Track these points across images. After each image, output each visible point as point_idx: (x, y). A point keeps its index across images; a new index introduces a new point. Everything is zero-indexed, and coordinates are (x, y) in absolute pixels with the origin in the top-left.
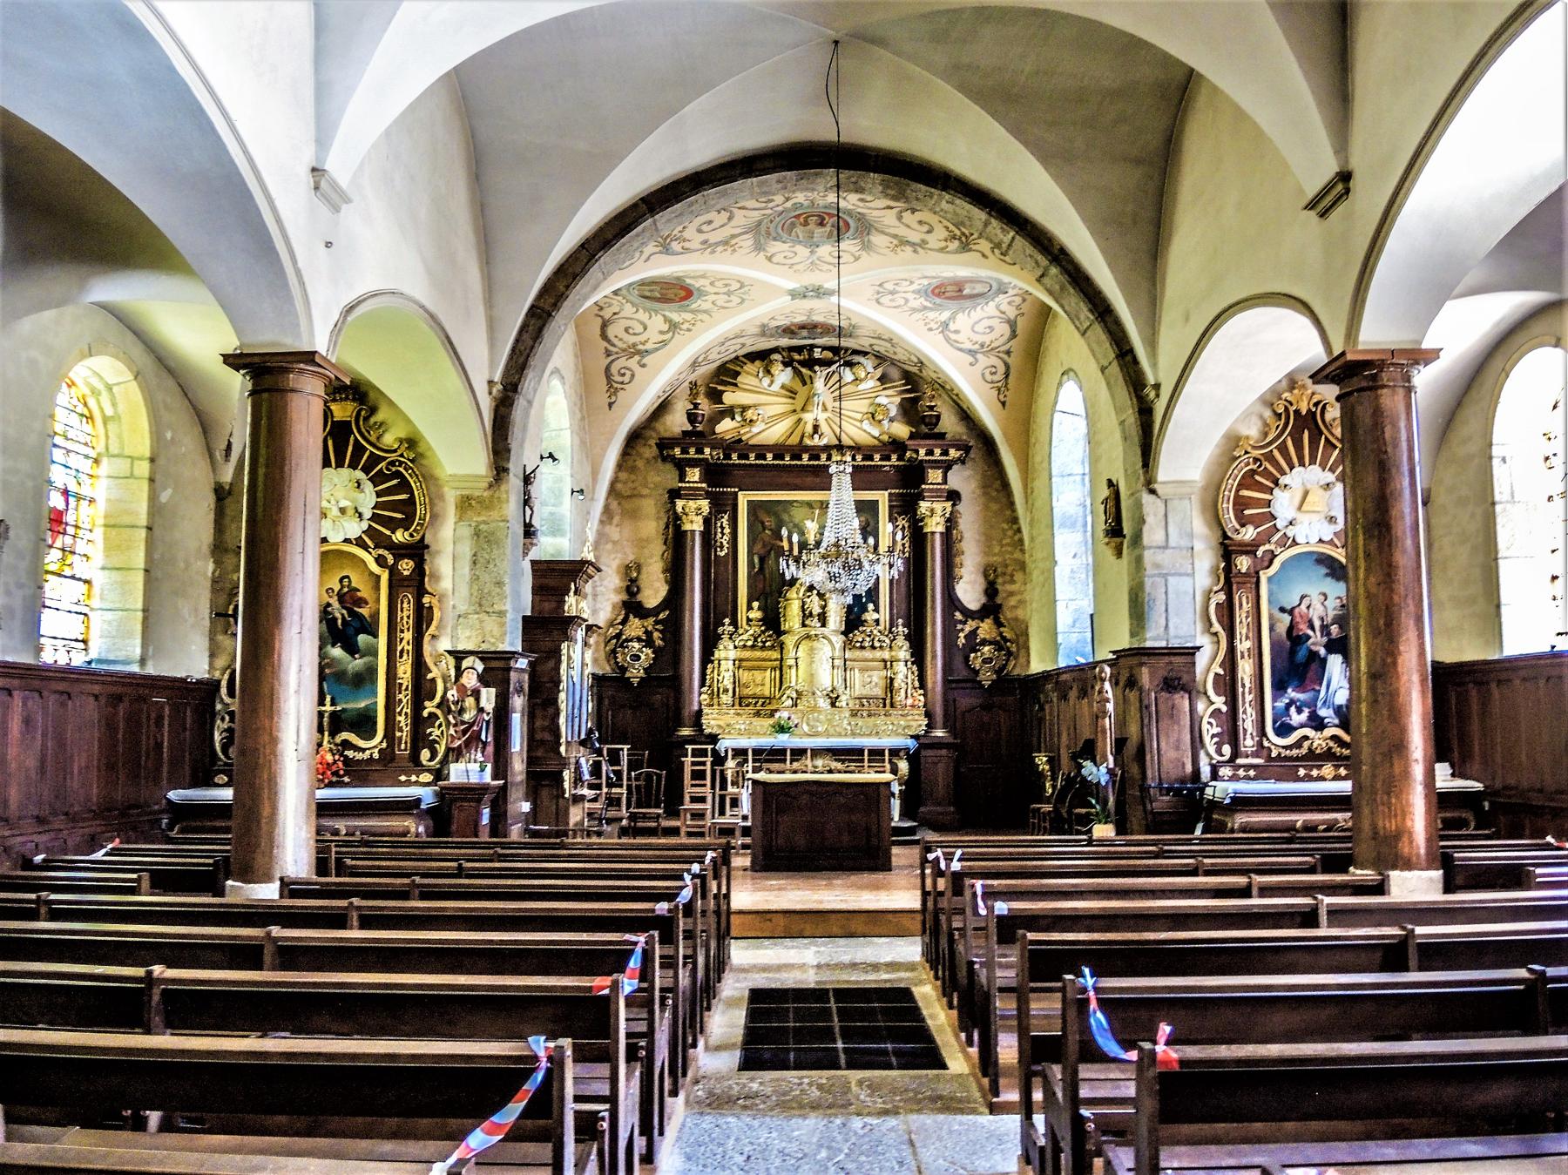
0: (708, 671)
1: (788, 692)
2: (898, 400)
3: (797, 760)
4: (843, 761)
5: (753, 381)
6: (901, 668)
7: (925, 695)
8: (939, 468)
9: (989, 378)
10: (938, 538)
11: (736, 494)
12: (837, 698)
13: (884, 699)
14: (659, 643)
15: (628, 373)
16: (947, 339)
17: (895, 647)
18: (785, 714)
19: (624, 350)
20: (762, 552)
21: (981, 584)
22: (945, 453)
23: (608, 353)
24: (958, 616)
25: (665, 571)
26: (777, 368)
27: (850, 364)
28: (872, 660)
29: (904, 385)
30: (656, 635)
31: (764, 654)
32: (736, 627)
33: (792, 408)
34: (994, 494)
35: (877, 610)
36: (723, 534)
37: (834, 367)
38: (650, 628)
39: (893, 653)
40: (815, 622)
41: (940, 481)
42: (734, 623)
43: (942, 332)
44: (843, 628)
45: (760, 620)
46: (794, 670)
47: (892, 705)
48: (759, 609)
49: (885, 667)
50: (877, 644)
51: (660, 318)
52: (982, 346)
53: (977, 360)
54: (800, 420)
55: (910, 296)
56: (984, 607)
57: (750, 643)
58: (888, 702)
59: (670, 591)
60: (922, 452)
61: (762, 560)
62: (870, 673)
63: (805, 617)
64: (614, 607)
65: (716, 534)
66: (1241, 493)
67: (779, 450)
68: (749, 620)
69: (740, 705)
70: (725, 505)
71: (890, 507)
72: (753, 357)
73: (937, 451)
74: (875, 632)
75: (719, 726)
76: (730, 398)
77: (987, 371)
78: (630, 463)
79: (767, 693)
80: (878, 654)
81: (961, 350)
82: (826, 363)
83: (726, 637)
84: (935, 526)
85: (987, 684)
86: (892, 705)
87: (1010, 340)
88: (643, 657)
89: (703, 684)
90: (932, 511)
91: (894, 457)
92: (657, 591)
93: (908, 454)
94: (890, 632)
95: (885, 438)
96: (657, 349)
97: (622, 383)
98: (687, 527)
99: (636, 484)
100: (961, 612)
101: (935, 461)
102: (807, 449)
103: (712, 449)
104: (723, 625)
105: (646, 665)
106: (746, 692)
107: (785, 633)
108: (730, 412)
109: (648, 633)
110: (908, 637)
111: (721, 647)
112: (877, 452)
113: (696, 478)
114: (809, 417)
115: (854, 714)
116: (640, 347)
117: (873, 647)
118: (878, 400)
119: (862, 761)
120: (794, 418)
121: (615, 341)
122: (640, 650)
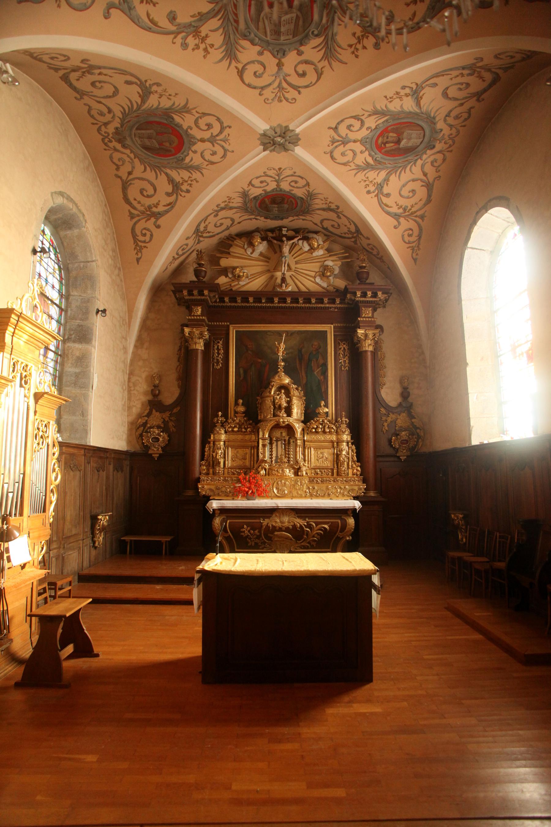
0: (207, 449)
2: (339, 263)
5: (241, 251)
6: (344, 446)
8: (370, 307)
9: (407, 239)
13: (332, 470)
14: (172, 429)
15: (148, 234)
16: (380, 203)
19: (143, 213)
21: (398, 390)
22: (375, 295)
23: (132, 216)
24: (383, 411)
26: (257, 240)
27: (306, 238)
28: (324, 441)
29: (343, 253)
30: (171, 424)
32: (227, 418)
35: (326, 406)
37: (295, 240)
38: (167, 419)
40: (283, 414)
41: (370, 315)
42: (225, 415)
43: (377, 195)
44: (303, 418)
45: (243, 413)
48: (243, 404)
49: (333, 447)
50: (327, 430)
51: (163, 178)
52: (405, 210)
53: (399, 223)
55: (358, 147)
56: (400, 405)
58: (335, 471)
59: (180, 394)
60: (359, 294)
61: (245, 372)
62: (322, 451)
64: (143, 405)
65: (214, 353)
67: (257, 296)
68: (236, 412)
72: (240, 235)
73: (369, 294)
74: (326, 421)
75: (211, 490)
76: (225, 262)
77: (406, 233)
80: (328, 437)
81: (388, 213)
82: (290, 238)
83: (219, 425)
84: (368, 346)
85: (156, 456)
86: (338, 474)
87: (425, 205)
88: (161, 439)
89: (202, 458)
90: (366, 336)
91: (338, 301)
93: (348, 296)
94: (336, 421)
95: (331, 289)
96: (167, 212)
97: (144, 242)
100: (385, 408)
101: (368, 302)
102: (277, 294)
103: (210, 291)
104: (218, 416)
105: (163, 445)
108: (225, 271)
109: (164, 422)
110: (349, 426)
112: (326, 296)
113: (199, 313)
114: (279, 275)
115: (311, 480)
116: (154, 209)
118: (327, 263)
121: (135, 203)
122: (159, 434)
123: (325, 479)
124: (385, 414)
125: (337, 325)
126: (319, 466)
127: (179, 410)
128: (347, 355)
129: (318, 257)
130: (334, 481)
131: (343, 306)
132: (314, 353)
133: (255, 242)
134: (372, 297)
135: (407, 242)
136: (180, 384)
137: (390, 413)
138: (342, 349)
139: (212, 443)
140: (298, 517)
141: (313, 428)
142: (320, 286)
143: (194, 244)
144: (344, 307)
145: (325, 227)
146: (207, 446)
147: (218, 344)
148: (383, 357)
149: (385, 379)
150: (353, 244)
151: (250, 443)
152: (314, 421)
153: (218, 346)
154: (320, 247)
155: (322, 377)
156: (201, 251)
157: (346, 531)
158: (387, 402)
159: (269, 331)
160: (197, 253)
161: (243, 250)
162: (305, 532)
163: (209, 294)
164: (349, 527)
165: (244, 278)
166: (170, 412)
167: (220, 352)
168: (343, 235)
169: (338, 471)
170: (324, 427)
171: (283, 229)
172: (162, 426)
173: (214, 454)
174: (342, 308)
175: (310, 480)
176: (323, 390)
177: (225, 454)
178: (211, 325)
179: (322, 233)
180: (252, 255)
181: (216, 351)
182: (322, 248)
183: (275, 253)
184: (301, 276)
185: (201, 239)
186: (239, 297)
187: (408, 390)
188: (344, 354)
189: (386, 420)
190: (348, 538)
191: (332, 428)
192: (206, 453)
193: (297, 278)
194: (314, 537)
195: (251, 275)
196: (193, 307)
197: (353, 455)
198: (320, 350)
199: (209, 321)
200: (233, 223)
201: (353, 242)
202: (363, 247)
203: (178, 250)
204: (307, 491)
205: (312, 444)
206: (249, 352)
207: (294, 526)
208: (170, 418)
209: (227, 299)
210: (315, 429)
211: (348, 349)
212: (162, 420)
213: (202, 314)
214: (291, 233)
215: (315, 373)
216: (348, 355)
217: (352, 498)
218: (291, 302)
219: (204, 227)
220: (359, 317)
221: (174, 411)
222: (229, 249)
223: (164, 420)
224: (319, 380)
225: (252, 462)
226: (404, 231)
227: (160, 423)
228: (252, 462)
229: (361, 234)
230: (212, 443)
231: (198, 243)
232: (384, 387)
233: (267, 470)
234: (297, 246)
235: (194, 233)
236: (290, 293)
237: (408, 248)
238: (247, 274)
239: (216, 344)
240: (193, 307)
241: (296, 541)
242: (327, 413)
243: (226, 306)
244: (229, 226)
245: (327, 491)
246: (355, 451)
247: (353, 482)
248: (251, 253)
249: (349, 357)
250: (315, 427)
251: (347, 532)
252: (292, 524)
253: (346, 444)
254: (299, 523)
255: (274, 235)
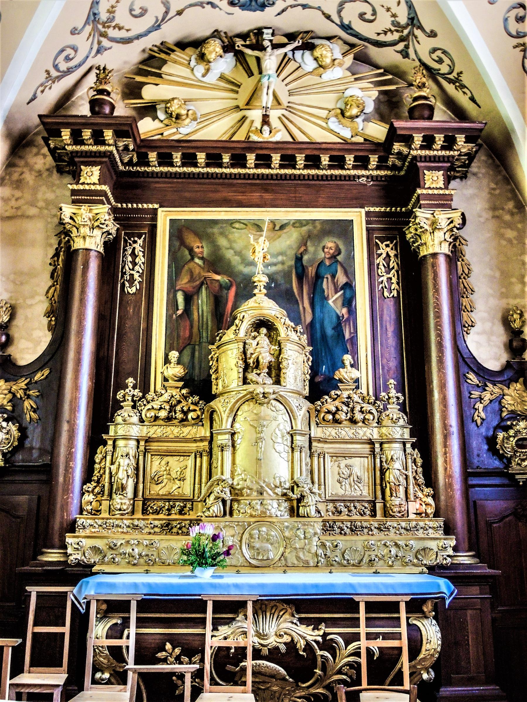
1: (217, 489)
2: (375, 94)
3: (228, 622)
4: (315, 623)
5: (184, 72)
7: (435, 497)
8: (438, 169)
10: (442, 262)
11: (155, 212)
12: (299, 501)
13: (373, 503)
17: (386, 422)
18: (209, 530)
20: (189, 288)
25: (48, 314)
30: (27, 404)
31: (188, 431)
32: (145, 389)
33: (234, 103)
34: (507, 217)
35: (355, 365)
36: (134, 264)
38: (20, 394)
39: (384, 430)
45: (181, 379)
46: (228, 454)
47: (386, 513)
48: (179, 363)
50: (359, 416)
54: (244, 119)
56: (508, 365)
57: (163, 414)
59: (442, 630)
61: (189, 299)
62: (349, 461)
63: (246, 368)
66: (20, 641)
69: (144, 511)
70: (142, 227)
71: (368, 229)
72: (182, 45)
75: (96, 550)
78: (15, 177)
79: (187, 490)
86: (386, 513)
89: (87, 478)
91: (374, 160)
92: (38, 343)
93: (397, 147)
94: (377, 398)
98: (78, 244)
99: (20, 202)
100: (477, 374)
104: (126, 387)
106: (156, 490)
107: (215, 397)
109: (15, 400)
111: (119, 419)
113: (95, 179)
117: (353, 421)
119: (355, 622)
120: (238, 115)
123: (359, 524)
124: (478, 386)
125: (372, 209)
126: (342, 497)
127: (47, 376)
128: (393, 268)
129: (332, 83)
130: (379, 529)
131: (382, 173)
132: (327, 263)
133: (211, 53)
134: (443, 148)
135: (514, 33)
136: (53, 323)
137: (489, 384)
138: (384, 255)
139: (110, 442)
140: (302, 621)
141: (329, 412)
142: (337, 135)
143: (90, 52)
144: (386, 176)
145: (346, 22)
146: (99, 451)
147: (135, 245)
148: (466, 271)
149: (472, 314)
150: (399, 56)
151: (195, 445)
152: (330, 397)
153: (134, 248)
154: (336, 62)
155: (344, 311)
156: (104, 69)
157: (421, 656)
158: (479, 361)
159: (238, 221)
160: (98, 72)
161: (189, 70)
162: (319, 659)
163: (115, 141)
164: (428, 646)
165: (188, 120)
166: (28, 380)
167: (137, 260)
168: (382, 38)
169: (385, 506)
170: (353, 410)
171: (265, 31)
172: (9, 408)
173: (114, 468)
174: (381, 177)
175: (324, 525)
176: (347, 336)
177: (137, 469)
178: (122, 208)
179: (340, 38)
180: (204, 79)
181: (130, 259)
182: (340, 65)
183: (250, 74)
184: (300, 117)
185: (105, 43)
186: (178, 152)
187: (522, 336)
188: (389, 266)
189: (481, 399)
190: (425, 676)
191: (370, 412)
192: (97, 466)
193: (291, 122)
194: (339, 672)
195: (202, 115)
196: (82, 167)
197: (416, 471)
198: (339, 258)
199: (116, 202)
200: (167, 13)
201: (400, 52)
202: (420, 60)
203: (55, 59)
204: (320, 551)
205: (327, 446)
206: (197, 260)
207: (291, 645)
208: (28, 392)
209: (153, 156)
210: (334, 414)
211: (396, 256)
212: (10, 396)
213: (101, 181)
214: (277, 39)
215: (330, 302)
216: (396, 267)
217: (425, 570)
218: (280, 165)
219: (109, 11)
220: (419, 187)
221: (36, 378)
222: (160, 68)
223: (14, 395)
224: (338, 317)
225: (197, 486)
226: (509, 11)
227: (5, 402)
228: (197, 486)
229: (421, 27)
230: (110, 442)
231: (98, 52)
232: (473, 330)
233: (228, 503)
234: (292, 62)
235: (87, 23)
236: (278, 146)
237: (515, 47)
238: (195, 113)
239: (130, 245)
240: (82, 167)
241: (296, 682)
242: (357, 381)
243: (153, 172)
244: (160, 18)
245: (367, 553)
246: (419, 461)
247: (421, 531)
248: (204, 76)
249: (397, 271)
250: (334, 409)
251: (424, 659)
252: (287, 639)
253: (401, 446)
254: (304, 638)
255: (248, 43)
